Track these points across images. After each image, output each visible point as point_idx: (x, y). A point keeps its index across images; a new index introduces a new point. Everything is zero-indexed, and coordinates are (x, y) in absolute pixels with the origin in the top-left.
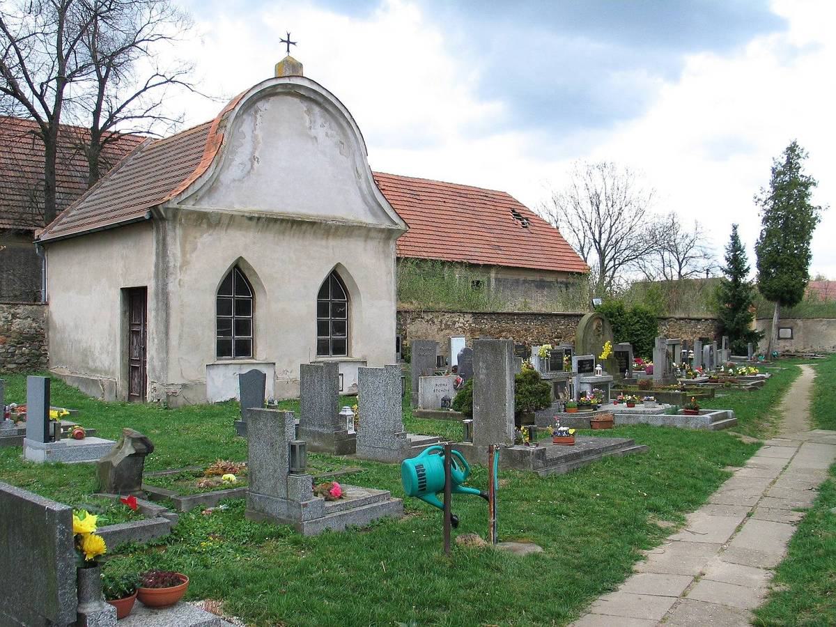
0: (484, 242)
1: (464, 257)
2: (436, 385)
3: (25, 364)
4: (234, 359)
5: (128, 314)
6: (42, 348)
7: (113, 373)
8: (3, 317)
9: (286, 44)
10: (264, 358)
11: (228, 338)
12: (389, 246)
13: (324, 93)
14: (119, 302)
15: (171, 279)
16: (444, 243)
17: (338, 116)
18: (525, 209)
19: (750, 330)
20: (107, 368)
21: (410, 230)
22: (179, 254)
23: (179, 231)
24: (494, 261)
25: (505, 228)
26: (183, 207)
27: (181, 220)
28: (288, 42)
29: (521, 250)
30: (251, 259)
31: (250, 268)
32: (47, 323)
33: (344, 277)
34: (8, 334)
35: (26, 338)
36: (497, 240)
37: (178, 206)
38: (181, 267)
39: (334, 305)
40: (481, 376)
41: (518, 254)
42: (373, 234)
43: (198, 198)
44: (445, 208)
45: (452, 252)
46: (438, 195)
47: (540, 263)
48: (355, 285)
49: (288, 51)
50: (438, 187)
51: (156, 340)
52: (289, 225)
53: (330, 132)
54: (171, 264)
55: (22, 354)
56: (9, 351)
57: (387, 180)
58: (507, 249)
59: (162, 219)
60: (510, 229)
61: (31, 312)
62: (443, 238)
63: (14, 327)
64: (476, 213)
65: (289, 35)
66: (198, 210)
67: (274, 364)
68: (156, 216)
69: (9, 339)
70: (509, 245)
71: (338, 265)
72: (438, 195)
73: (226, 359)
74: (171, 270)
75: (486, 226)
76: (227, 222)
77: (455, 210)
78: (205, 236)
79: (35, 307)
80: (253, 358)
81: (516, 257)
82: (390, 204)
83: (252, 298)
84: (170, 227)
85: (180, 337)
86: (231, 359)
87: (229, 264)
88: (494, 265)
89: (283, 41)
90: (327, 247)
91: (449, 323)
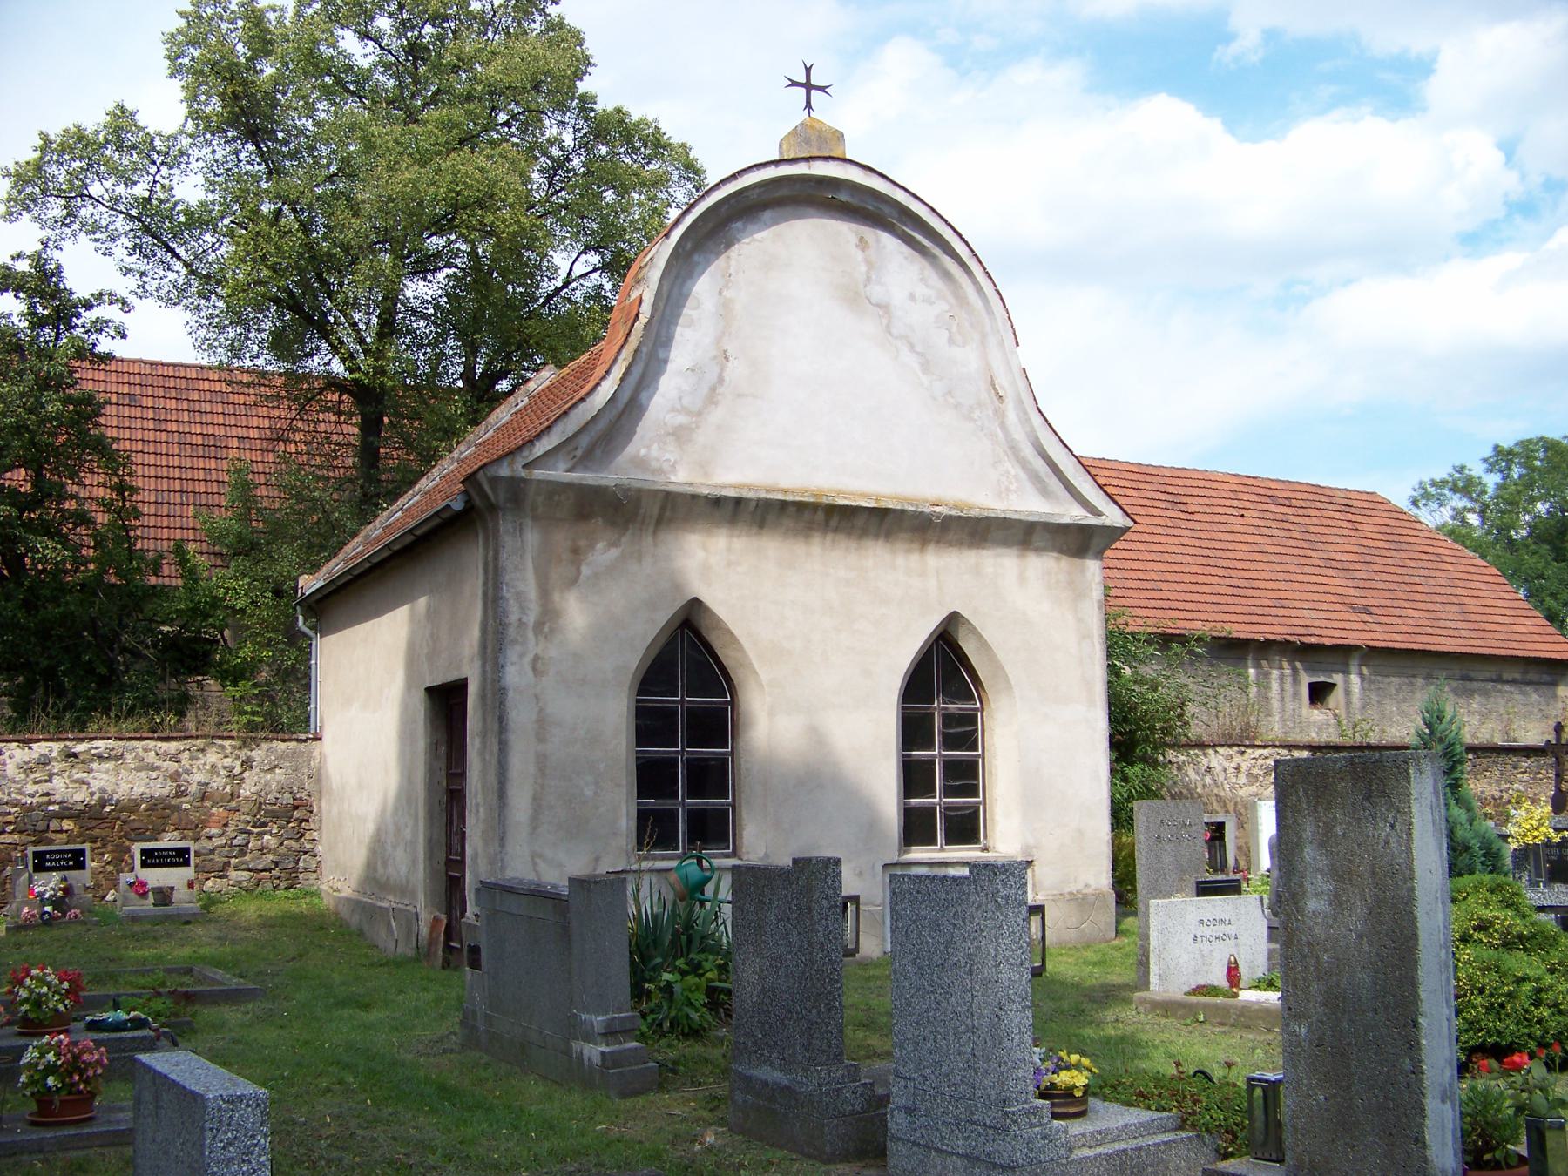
0: (1333, 598)
1: (1290, 630)
2: (1201, 922)
3: (270, 870)
4: (942, 849)
5: (443, 749)
6: (307, 836)
7: (413, 894)
8: (225, 768)
9: (803, 90)
11: (667, 804)
12: (1083, 571)
13: (900, 196)
14: (422, 723)
15: (512, 654)
16: (1244, 601)
17: (937, 251)
18: (1418, 526)
20: (404, 882)
22: (532, 592)
23: (532, 537)
24: (1354, 638)
25: (1376, 568)
26: (538, 474)
28: (808, 87)
29: (1416, 614)
30: (722, 600)
31: (718, 623)
32: (319, 781)
33: (969, 647)
34: (234, 804)
35: (274, 815)
36: (1362, 592)
37: (523, 473)
38: (539, 626)
39: (694, 714)
40: (1311, 905)
41: (1411, 622)
42: (1038, 540)
43: (579, 453)
44: (1242, 529)
45: (1260, 620)
46: (1228, 503)
47: (1460, 641)
48: (998, 667)
49: (808, 105)
50: (1226, 487)
51: (481, 810)
52: (820, 516)
53: (921, 290)
54: (513, 618)
55: (263, 850)
56: (235, 842)
57: (1115, 474)
58: (1384, 611)
59: (493, 508)
60: (1388, 569)
61: (284, 756)
62: (1243, 592)
63: (246, 791)
64: (1312, 538)
65: (808, 70)
66: (576, 481)
68: (477, 501)
70: (1388, 603)
71: (953, 619)
72: (1228, 503)
73: (664, 858)
74: (512, 632)
75: (1334, 564)
76: (656, 511)
77: (1267, 531)
78: (600, 546)
79: (293, 745)
81: (1404, 629)
82: (1101, 487)
83: (733, 703)
84: (510, 526)
85: (537, 799)
86: (727, 856)
87: (663, 616)
88: (1357, 648)
91: (1255, 771)
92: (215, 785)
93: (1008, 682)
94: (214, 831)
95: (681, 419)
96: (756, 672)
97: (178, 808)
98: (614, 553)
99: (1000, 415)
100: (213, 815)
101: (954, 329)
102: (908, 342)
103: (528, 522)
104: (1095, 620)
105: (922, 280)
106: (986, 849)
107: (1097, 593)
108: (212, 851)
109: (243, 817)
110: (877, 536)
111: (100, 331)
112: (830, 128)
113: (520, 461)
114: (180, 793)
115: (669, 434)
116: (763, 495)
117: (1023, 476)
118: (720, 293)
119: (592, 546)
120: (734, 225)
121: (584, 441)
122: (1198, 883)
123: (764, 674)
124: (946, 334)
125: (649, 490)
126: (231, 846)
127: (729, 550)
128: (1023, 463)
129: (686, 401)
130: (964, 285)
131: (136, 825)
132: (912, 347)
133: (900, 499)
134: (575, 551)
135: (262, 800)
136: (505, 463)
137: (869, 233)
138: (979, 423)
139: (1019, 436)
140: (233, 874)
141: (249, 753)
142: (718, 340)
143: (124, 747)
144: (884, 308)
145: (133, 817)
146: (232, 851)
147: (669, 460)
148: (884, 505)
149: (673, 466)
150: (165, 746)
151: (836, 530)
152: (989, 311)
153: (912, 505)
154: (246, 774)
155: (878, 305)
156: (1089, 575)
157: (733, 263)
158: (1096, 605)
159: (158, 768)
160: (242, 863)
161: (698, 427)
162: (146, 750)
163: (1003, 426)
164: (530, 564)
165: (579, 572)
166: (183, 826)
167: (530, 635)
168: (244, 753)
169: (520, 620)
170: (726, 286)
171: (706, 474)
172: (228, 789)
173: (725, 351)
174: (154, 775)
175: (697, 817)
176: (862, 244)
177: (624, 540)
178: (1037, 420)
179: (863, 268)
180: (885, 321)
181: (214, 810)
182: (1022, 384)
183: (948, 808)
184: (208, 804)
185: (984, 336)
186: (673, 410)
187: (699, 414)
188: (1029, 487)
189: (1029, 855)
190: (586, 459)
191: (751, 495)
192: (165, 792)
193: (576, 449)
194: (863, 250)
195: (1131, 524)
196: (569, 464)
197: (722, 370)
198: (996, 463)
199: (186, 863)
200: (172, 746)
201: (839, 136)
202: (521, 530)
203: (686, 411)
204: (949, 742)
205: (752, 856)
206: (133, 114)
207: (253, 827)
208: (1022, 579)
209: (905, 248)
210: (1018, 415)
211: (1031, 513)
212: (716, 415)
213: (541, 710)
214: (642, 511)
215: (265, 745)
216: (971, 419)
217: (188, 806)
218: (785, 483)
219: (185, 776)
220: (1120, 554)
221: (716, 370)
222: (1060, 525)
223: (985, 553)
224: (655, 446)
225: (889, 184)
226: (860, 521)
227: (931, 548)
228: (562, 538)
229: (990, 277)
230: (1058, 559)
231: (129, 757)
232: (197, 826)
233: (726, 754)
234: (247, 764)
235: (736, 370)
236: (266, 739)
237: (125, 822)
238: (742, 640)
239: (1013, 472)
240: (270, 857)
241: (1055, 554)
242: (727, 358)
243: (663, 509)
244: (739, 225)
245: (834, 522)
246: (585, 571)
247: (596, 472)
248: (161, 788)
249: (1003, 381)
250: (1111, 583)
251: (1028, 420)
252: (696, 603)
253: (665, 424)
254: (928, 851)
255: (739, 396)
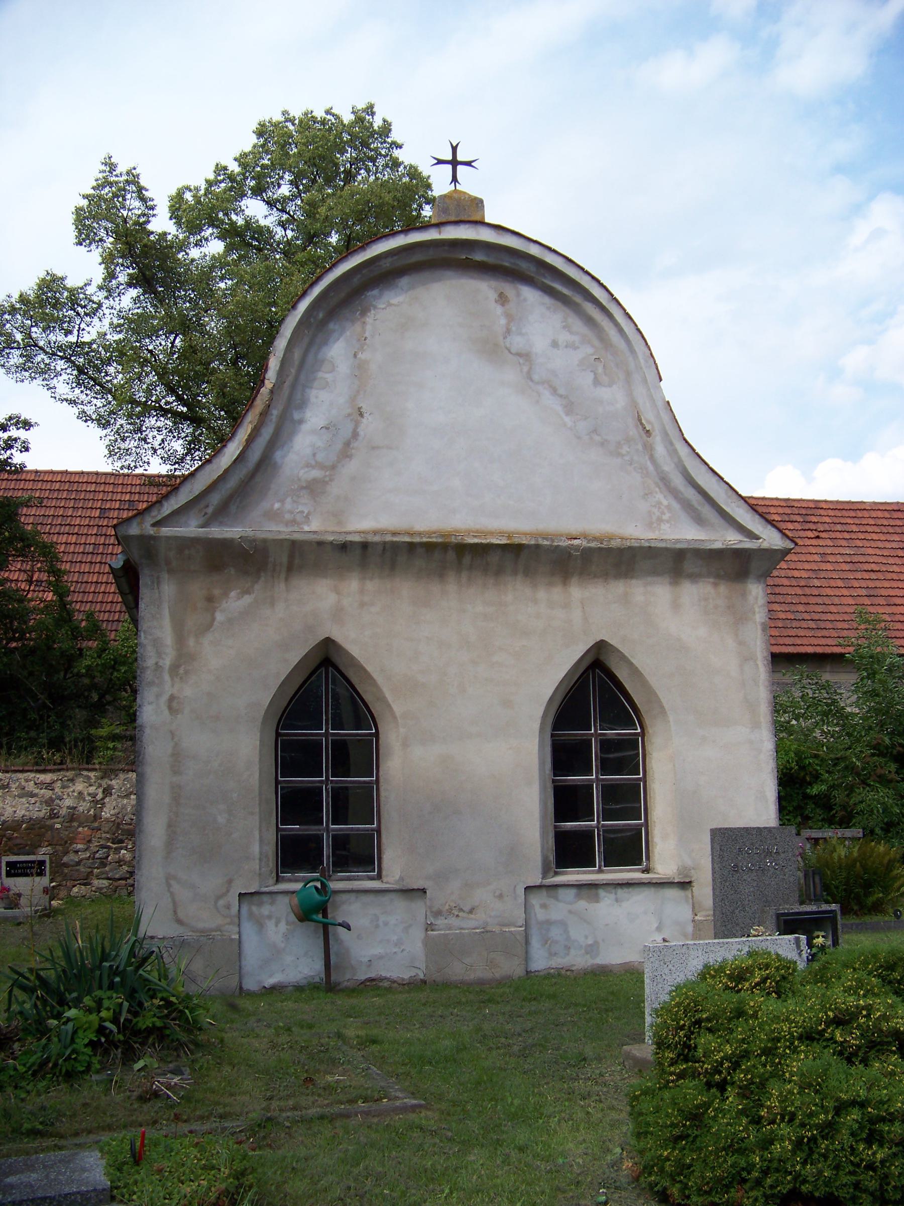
4: (600, 871)
8: (89, 794)
10: (397, 877)
11: (312, 830)
12: (744, 595)
13: (534, 250)
17: (578, 299)
19: (294, 412)
21: (798, 549)
27: (168, 563)
28: (454, 163)
34: (96, 824)
37: (151, 531)
38: (174, 669)
39: (607, 745)
43: (210, 510)
49: (455, 179)
52: (451, 555)
53: (564, 337)
54: (150, 662)
56: (97, 855)
63: (106, 814)
67: (424, 891)
69: (98, 835)
76: (285, 560)
78: (233, 594)
80: (379, 877)
85: (171, 825)
86: (372, 879)
89: (468, 164)
90: (566, 606)
92: (81, 809)
93: (662, 707)
94: (80, 846)
95: (316, 473)
96: (389, 706)
97: (51, 828)
98: (247, 599)
99: (649, 449)
100: (80, 833)
101: (600, 370)
102: (551, 386)
103: (165, 576)
104: (759, 642)
105: (564, 327)
106: (647, 870)
107: (760, 616)
108: (78, 863)
109: (104, 835)
110: (515, 573)
111: (11, 447)
112: (470, 196)
113: (149, 520)
114: (53, 815)
115: (302, 488)
116: (389, 538)
117: (676, 506)
118: (355, 356)
119: (226, 594)
120: (369, 293)
121: (215, 499)
122: (778, 916)
123: (398, 708)
124: (592, 376)
125: (274, 540)
126: (94, 858)
127: (362, 591)
128: (674, 493)
129: (320, 457)
130: (606, 328)
131: (18, 841)
132: (554, 391)
133: (532, 535)
134: (210, 599)
135: (119, 820)
136: (135, 523)
137: (510, 289)
138: (627, 458)
139: (668, 467)
140: (96, 882)
141: (110, 782)
142: (353, 399)
143: (10, 778)
144: (525, 356)
145: (16, 835)
146: (93, 863)
147: (302, 512)
148: (516, 541)
149: (307, 517)
150: (42, 777)
151: (471, 568)
152: (632, 351)
153: (546, 539)
154: (107, 800)
155: (519, 355)
156: (751, 599)
157: (369, 328)
158: (759, 628)
159: (35, 795)
160: (102, 873)
161: (331, 480)
162: (27, 781)
163: (652, 458)
164: (166, 612)
165: (213, 619)
166: (55, 842)
167: (167, 677)
168: (105, 783)
169: (156, 664)
170: (362, 349)
171: (340, 523)
172: (92, 812)
173: (360, 408)
174: (33, 800)
175: (340, 842)
176: (502, 299)
177: (257, 587)
178: (683, 451)
179: (503, 321)
180: (525, 369)
181: (80, 829)
182: (666, 418)
183: (608, 831)
184: (75, 824)
185: (628, 374)
186: (308, 465)
187: (333, 467)
188: (683, 516)
189: (686, 876)
190: (221, 513)
191: (377, 539)
192: (41, 814)
193: (207, 506)
194: (503, 305)
195: (792, 546)
196: (201, 520)
197: (357, 424)
198: (646, 495)
199: (41, 874)
200: (47, 777)
201: (478, 203)
202: (159, 583)
203: (321, 466)
204: (605, 767)
205: (390, 879)
206: (63, 279)
207: (113, 843)
208: (676, 606)
209: (547, 300)
210: (666, 447)
211: (678, 541)
212: (351, 467)
213: (176, 745)
214: (271, 559)
215: (122, 776)
216: (619, 455)
217: (58, 826)
218: (420, 526)
219: (58, 801)
220: (783, 573)
221: (350, 426)
222: (711, 551)
223: (634, 581)
224: (289, 500)
225: (522, 240)
226: (494, 558)
227: (574, 580)
228: (197, 588)
229: (630, 318)
230: (715, 585)
231: (13, 786)
232: (66, 842)
233: (371, 782)
234: (107, 792)
235: (370, 426)
236: (123, 770)
237: (10, 839)
238: (375, 676)
239: (665, 503)
240: (125, 868)
241: (712, 580)
242: (361, 415)
243: (291, 557)
244: (375, 292)
245: (467, 559)
246: (219, 617)
247: (231, 526)
248: (38, 812)
249: (649, 416)
250: (776, 607)
251: (675, 451)
252: (328, 643)
253: (299, 480)
254: (585, 873)
255: (374, 448)
